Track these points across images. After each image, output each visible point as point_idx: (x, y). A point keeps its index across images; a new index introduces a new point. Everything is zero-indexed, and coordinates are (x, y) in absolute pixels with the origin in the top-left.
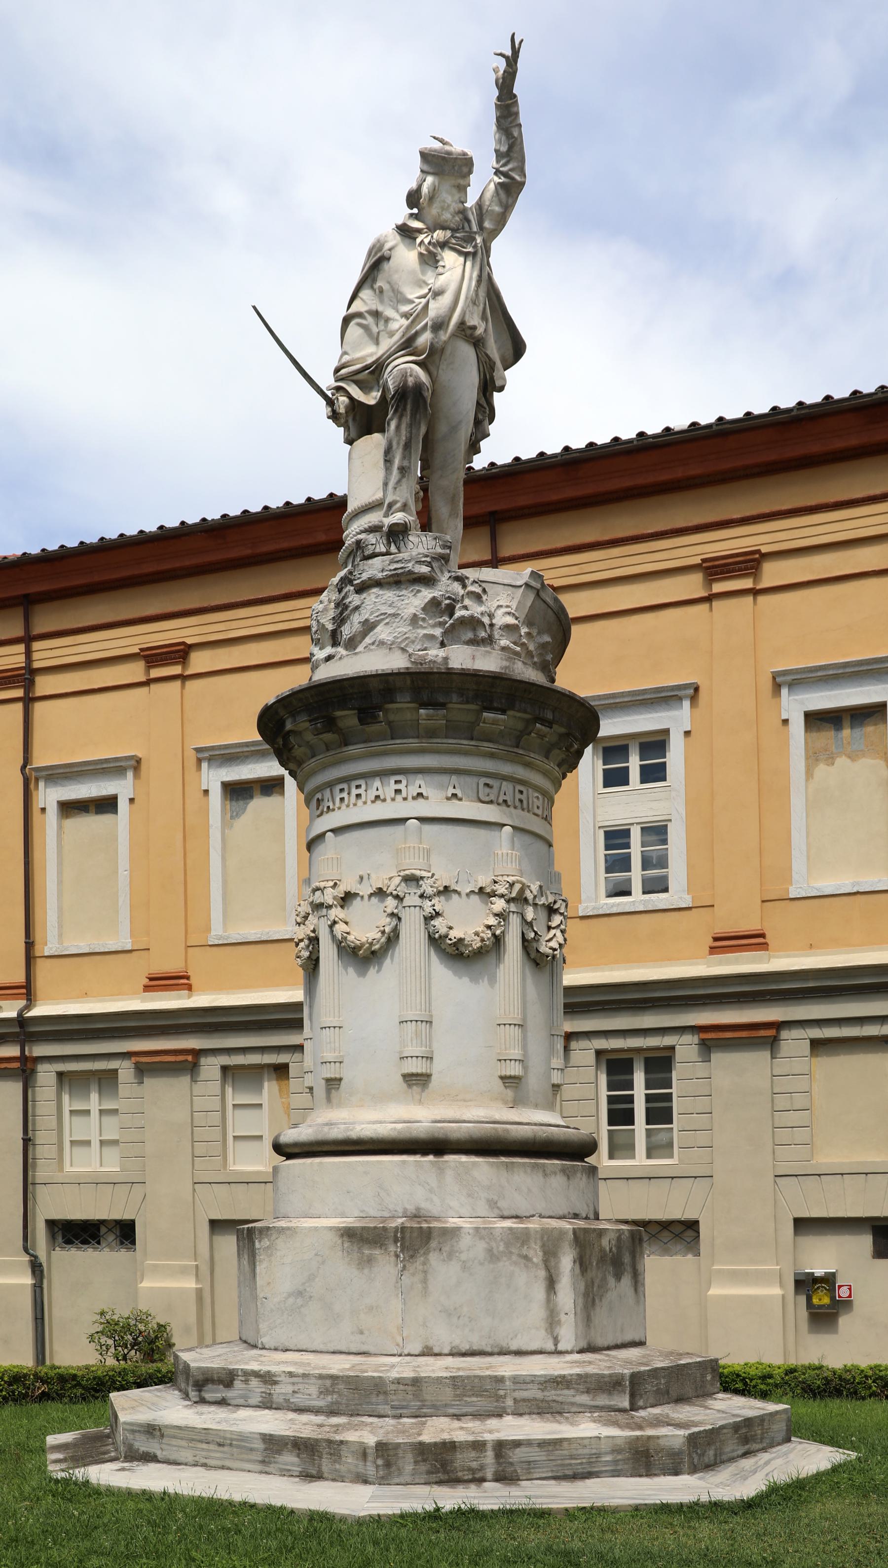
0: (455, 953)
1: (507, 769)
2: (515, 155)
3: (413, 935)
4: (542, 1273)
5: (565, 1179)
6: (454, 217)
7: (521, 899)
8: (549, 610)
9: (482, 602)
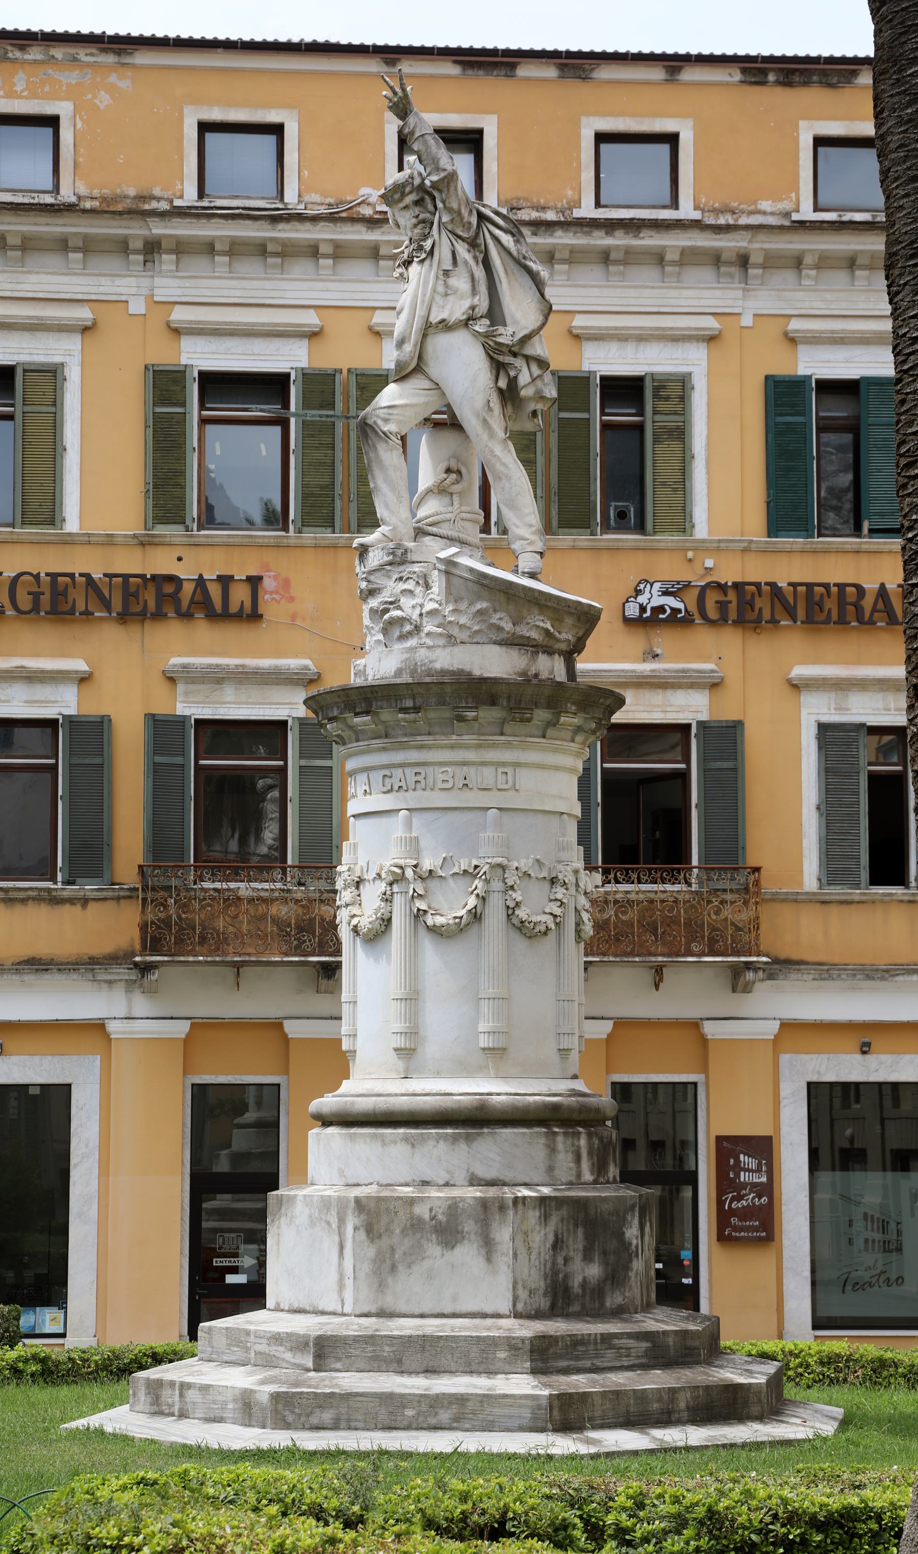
0: (525, 930)
1: (398, 757)
3: (495, 916)
4: (337, 1238)
5: (409, 1147)
7: (398, 879)
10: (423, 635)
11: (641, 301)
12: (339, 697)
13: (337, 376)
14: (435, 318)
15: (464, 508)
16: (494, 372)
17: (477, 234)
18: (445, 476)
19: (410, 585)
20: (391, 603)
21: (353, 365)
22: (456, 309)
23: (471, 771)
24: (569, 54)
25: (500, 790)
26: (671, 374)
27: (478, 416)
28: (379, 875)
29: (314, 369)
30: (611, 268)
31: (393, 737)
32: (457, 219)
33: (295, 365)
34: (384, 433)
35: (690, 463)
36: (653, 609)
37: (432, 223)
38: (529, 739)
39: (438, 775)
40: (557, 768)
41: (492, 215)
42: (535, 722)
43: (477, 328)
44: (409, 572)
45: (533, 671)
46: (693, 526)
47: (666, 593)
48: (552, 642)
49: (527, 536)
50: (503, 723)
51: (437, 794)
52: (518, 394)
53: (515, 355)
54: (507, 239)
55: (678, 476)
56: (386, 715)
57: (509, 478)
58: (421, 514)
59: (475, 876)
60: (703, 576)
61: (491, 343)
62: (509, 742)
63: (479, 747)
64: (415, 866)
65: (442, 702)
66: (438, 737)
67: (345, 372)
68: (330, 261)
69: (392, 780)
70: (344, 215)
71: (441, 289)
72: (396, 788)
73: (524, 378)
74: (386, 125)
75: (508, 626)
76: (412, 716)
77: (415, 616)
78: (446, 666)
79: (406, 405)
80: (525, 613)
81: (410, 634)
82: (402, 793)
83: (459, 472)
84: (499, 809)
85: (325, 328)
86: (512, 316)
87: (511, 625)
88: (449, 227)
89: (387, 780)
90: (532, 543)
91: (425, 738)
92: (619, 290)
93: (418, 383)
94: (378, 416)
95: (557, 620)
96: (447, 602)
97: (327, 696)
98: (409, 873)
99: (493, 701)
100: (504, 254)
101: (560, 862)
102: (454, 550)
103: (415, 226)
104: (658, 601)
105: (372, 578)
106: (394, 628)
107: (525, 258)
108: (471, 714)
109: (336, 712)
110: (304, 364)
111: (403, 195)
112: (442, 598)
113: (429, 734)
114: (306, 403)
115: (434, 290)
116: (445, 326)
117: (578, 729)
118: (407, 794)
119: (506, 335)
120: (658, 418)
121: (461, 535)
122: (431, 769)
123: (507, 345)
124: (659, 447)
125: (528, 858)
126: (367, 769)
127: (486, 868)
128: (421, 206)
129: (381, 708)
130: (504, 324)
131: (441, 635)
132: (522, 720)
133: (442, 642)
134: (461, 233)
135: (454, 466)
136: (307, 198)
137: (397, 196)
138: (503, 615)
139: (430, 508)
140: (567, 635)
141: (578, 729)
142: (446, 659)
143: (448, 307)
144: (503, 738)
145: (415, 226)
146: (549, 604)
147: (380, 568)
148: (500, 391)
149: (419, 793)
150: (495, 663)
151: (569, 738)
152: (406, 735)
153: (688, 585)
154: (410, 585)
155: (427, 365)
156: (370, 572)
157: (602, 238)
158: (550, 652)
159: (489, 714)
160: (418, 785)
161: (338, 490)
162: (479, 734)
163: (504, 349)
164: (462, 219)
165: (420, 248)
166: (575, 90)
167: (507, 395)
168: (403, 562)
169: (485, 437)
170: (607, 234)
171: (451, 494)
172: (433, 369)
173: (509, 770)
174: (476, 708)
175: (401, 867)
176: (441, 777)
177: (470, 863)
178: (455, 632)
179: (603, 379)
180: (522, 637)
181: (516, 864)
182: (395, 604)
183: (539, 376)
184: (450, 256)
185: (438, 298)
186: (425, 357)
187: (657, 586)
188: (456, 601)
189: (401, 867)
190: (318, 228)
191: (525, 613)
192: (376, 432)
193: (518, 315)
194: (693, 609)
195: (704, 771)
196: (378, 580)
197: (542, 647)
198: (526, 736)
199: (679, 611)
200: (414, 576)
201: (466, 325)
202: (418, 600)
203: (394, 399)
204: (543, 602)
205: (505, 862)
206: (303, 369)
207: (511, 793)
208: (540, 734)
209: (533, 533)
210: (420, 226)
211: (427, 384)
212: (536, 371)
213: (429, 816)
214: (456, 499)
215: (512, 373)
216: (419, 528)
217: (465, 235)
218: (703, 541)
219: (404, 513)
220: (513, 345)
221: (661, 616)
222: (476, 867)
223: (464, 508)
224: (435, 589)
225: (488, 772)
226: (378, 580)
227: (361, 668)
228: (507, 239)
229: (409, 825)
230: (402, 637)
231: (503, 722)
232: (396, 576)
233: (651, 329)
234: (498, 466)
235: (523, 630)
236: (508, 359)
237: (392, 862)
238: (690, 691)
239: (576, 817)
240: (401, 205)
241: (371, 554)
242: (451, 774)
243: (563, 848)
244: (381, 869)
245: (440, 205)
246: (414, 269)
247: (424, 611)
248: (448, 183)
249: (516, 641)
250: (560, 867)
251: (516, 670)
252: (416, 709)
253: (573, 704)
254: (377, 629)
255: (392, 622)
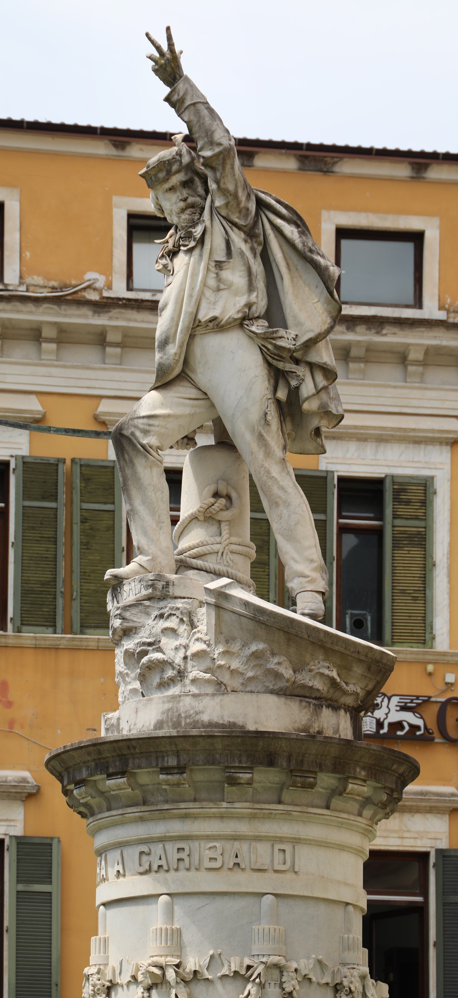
1: (158, 829)
2: (197, 135)
6: (179, 217)
8: (242, 618)
9: (178, 635)
10: (187, 681)
11: (381, 401)
12: (89, 754)
13: (60, 466)
14: (204, 315)
15: (234, 539)
16: (272, 381)
17: (255, 223)
18: (212, 500)
19: (172, 623)
20: (150, 644)
21: (77, 455)
22: (229, 306)
23: (243, 847)
24: (310, 147)
25: (276, 871)
26: (412, 477)
27: (253, 430)
28: (134, 978)
29: (36, 458)
30: (351, 365)
31: (153, 804)
32: (233, 203)
33: (15, 452)
34: (143, 446)
35: (431, 570)
36: (390, 724)
37: (203, 209)
38: (311, 810)
39: (204, 851)
40: (342, 847)
41: (273, 202)
42: (318, 789)
43: (254, 329)
44: (171, 609)
45: (315, 728)
46: (434, 638)
47: (404, 708)
48: (337, 694)
49: (307, 572)
50: (281, 790)
51: (203, 875)
52: (300, 407)
53: (297, 362)
54: (290, 230)
55: (418, 585)
56: (145, 776)
57: (287, 504)
58: (183, 544)
59: (247, 980)
60: (443, 692)
61: (270, 347)
62: (288, 813)
63: (252, 817)
64: (178, 966)
65: (211, 761)
66: (205, 804)
67: (68, 462)
68: (54, 346)
69: (151, 858)
70: (69, 298)
71: (212, 282)
72: (155, 867)
73: (308, 389)
74: (115, 210)
75: (287, 672)
76: (177, 777)
77: (178, 660)
78: (215, 719)
79: (168, 416)
80: (308, 657)
81: (172, 681)
82: (162, 874)
83: (229, 497)
84: (276, 895)
85: (48, 416)
86: (295, 317)
87: (291, 672)
88: (224, 213)
89: (145, 858)
90: (312, 581)
91: (191, 805)
92: (359, 388)
93: (184, 390)
94: (136, 427)
95: (344, 668)
96: (217, 642)
97: (74, 753)
98: (171, 974)
99: (270, 761)
100: (286, 247)
101: (344, 964)
102: (225, 581)
103: (183, 211)
104: (395, 716)
105: (127, 615)
106: (155, 674)
107: (311, 251)
108: (245, 776)
109: (84, 774)
110: (25, 451)
111: (169, 174)
112: (211, 637)
113: (195, 800)
114: (26, 493)
115: (204, 284)
116: (217, 325)
117: (367, 801)
118: (168, 875)
119: (287, 339)
120: (398, 522)
121: (230, 570)
122: (196, 844)
123: (289, 350)
124: (399, 553)
125: (308, 958)
126: (121, 845)
127: (260, 969)
128: (189, 187)
129: (140, 767)
130: (286, 327)
131: (208, 681)
132: (303, 786)
133: (210, 690)
134: (237, 220)
135: (223, 489)
136: (29, 280)
137: (161, 175)
138: (282, 659)
139: (194, 538)
140: (355, 687)
141: (367, 801)
142: (215, 710)
143: (220, 304)
144: (280, 807)
145: (183, 211)
146: (337, 648)
147: (137, 604)
148: (278, 402)
149: (182, 873)
150: (272, 715)
151: (356, 812)
152: (167, 802)
153: (427, 701)
154: (172, 623)
155: (193, 371)
156: (126, 608)
157: (343, 333)
158: (335, 707)
159: (266, 777)
160: (181, 864)
161: (60, 584)
162: (253, 801)
163: (285, 355)
164: (239, 203)
165: (189, 236)
166: (316, 183)
167: (286, 410)
168: (164, 597)
169: (260, 455)
170: (348, 329)
171: (219, 522)
172: (202, 376)
173: (288, 847)
174: (251, 768)
175: (161, 968)
176: (209, 854)
177: (242, 963)
178: (226, 678)
179: (341, 479)
180: (304, 686)
181: (294, 965)
182: (154, 645)
183: (325, 388)
184: (223, 246)
185: (208, 293)
186: (191, 362)
187: (395, 700)
188: (227, 642)
189: (161, 968)
190: (41, 309)
191: (308, 657)
192: (134, 445)
193: (302, 316)
194: (433, 726)
195: (442, 904)
196: (134, 616)
197: (326, 700)
198: (307, 806)
199: (418, 728)
200: (178, 613)
201: (241, 325)
202: (182, 641)
203: (155, 408)
204: (329, 645)
205: (282, 961)
206: (23, 457)
207: (289, 876)
208: (324, 804)
209: (314, 570)
210: (188, 211)
211: (193, 393)
212: (321, 382)
213: (195, 902)
214: (225, 528)
215: (294, 383)
216: (181, 561)
217: (241, 222)
218: (444, 654)
219: (165, 541)
220: (295, 351)
221: (399, 733)
222: (249, 967)
223: (234, 539)
224: (202, 627)
225: (263, 849)
226: (134, 616)
227: (114, 721)
228: (290, 230)
229: (170, 914)
230: (164, 685)
231: (281, 788)
232: (156, 613)
233: (392, 429)
234: (276, 490)
235: (305, 679)
236: (289, 366)
237: (150, 961)
238: (429, 816)
239: (362, 909)
240: (167, 186)
241: (126, 588)
242: (219, 851)
243: (348, 947)
244: (138, 970)
245: (212, 186)
246: (181, 260)
247: (189, 653)
248: (224, 160)
249: (296, 692)
250: (345, 970)
251: (296, 725)
252: (181, 769)
253: (363, 768)
254: (133, 675)
255: (152, 666)
